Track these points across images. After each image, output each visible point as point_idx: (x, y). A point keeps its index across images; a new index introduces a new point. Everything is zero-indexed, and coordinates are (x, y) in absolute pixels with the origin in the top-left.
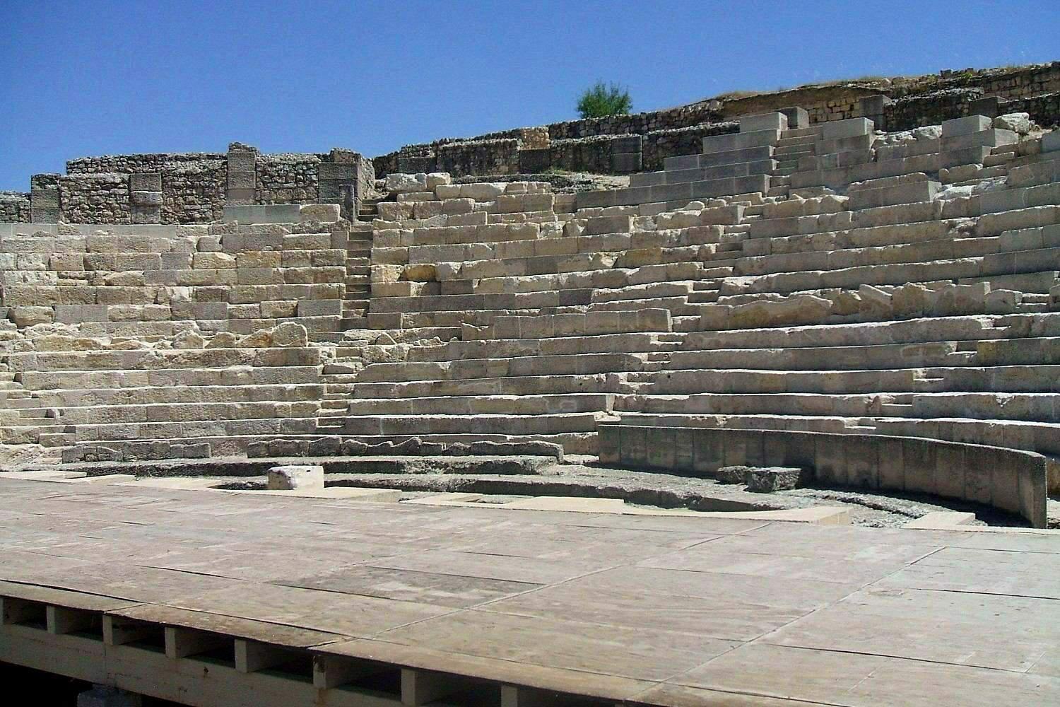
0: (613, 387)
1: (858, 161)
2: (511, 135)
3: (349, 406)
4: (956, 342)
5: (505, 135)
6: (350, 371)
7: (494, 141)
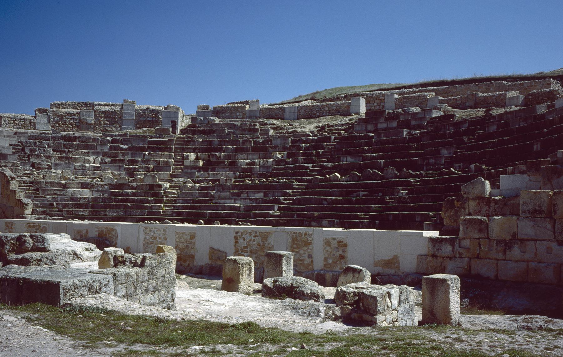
0: (277, 201)
1: (531, 86)
2: (243, 103)
3: (174, 206)
4: (484, 109)
5: (241, 103)
6: (174, 193)
7: (236, 105)
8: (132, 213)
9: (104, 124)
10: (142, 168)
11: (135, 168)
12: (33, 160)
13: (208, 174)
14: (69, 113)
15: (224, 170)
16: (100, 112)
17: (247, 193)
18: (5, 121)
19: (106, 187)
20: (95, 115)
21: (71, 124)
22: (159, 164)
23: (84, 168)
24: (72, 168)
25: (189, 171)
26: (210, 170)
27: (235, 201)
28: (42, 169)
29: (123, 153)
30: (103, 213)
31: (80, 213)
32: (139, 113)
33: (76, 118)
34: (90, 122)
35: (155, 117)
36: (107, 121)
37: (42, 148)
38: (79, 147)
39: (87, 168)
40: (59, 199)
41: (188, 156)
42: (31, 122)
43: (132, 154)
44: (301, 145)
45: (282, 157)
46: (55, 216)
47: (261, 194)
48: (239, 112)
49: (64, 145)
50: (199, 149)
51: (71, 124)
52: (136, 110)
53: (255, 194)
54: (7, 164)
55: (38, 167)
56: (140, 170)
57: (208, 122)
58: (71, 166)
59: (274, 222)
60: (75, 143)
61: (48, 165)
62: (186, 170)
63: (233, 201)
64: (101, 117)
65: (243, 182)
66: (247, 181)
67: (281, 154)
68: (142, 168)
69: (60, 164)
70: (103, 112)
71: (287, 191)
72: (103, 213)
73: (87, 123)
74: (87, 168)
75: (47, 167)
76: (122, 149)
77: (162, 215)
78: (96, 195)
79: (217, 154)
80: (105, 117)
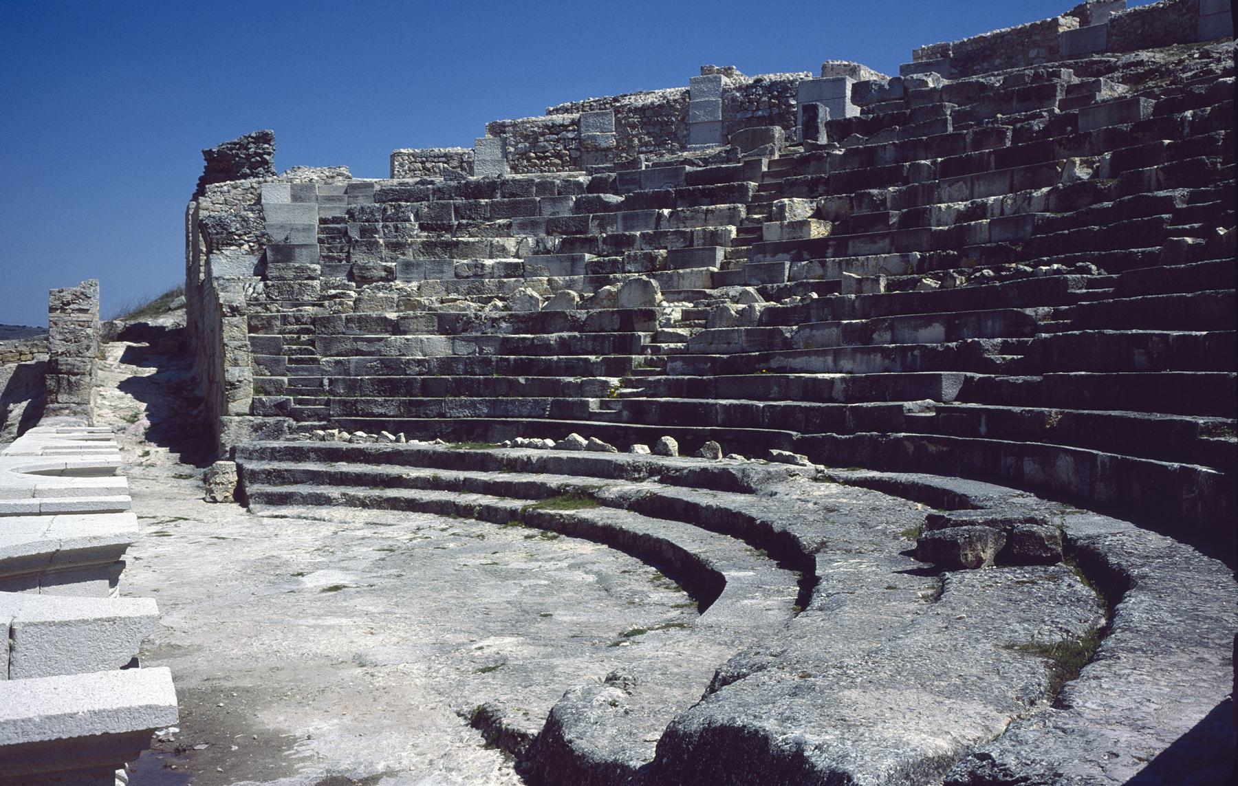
8: (510, 407)
9: (642, 144)
10: (634, 259)
11: (616, 261)
12: (359, 258)
13: (823, 264)
14: (554, 125)
15: (875, 247)
16: (630, 111)
17: (891, 328)
18: (401, 165)
19: (504, 325)
20: (618, 121)
21: (558, 155)
22: (691, 244)
23: (479, 272)
24: (449, 275)
25: (769, 260)
26: (830, 251)
27: (835, 361)
28: (368, 280)
29: (602, 219)
30: (435, 409)
31: (375, 410)
32: (734, 99)
33: (570, 135)
34: (604, 145)
35: (779, 106)
36: (648, 134)
37: (391, 224)
38: (496, 210)
39: (488, 270)
40: (352, 366)
41: (782, 208)
42: (462, 162)
43: (625, 218)
44: (1178, 117)
45: (1096, 174)
46: (309, 417)
47: (938, 330)
48: (1035, 44)
49: (457, 209)
50: (826, 182)
51: (558, 155)
52: (725, 91)
53: (916, 328)
54: (283, 273)
55: (360, 277)
56: (628, 267)
57: (906, 90)
58: (446, 268)
59: (910, 448)
60: (483, 201)
61: (386, 269)
62: (760, 256)
63: (830, 359)
64: (633, 126)
65: (914, 283)
66: (928, 281)
67: (1089, 164)
68: (634, 259)
69: (419, 265)
70: (637, 110)
71: (1029, 311)
72: (435, 409)
73: (597, 149)
74: (488, 270)
75: (384, 274)
76: (607, 206)
77: (592, 416)
78: (463, 350)
79: (875, 191)
80: (643, 124)
